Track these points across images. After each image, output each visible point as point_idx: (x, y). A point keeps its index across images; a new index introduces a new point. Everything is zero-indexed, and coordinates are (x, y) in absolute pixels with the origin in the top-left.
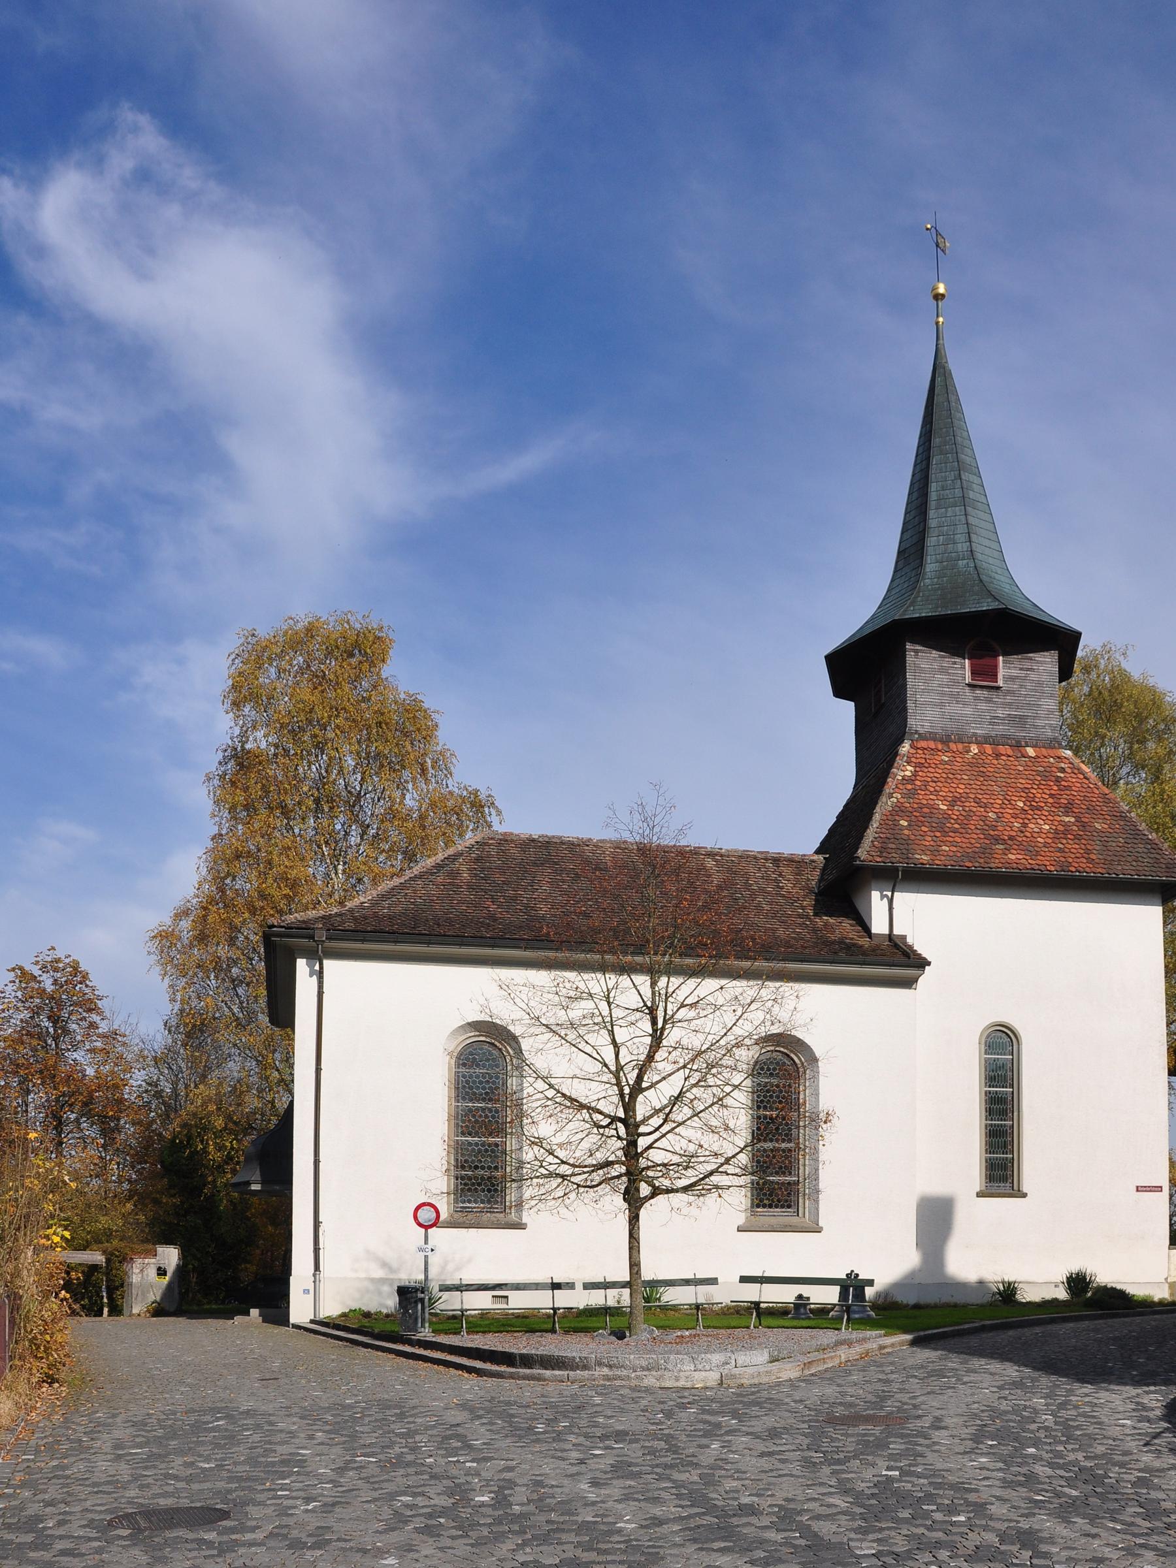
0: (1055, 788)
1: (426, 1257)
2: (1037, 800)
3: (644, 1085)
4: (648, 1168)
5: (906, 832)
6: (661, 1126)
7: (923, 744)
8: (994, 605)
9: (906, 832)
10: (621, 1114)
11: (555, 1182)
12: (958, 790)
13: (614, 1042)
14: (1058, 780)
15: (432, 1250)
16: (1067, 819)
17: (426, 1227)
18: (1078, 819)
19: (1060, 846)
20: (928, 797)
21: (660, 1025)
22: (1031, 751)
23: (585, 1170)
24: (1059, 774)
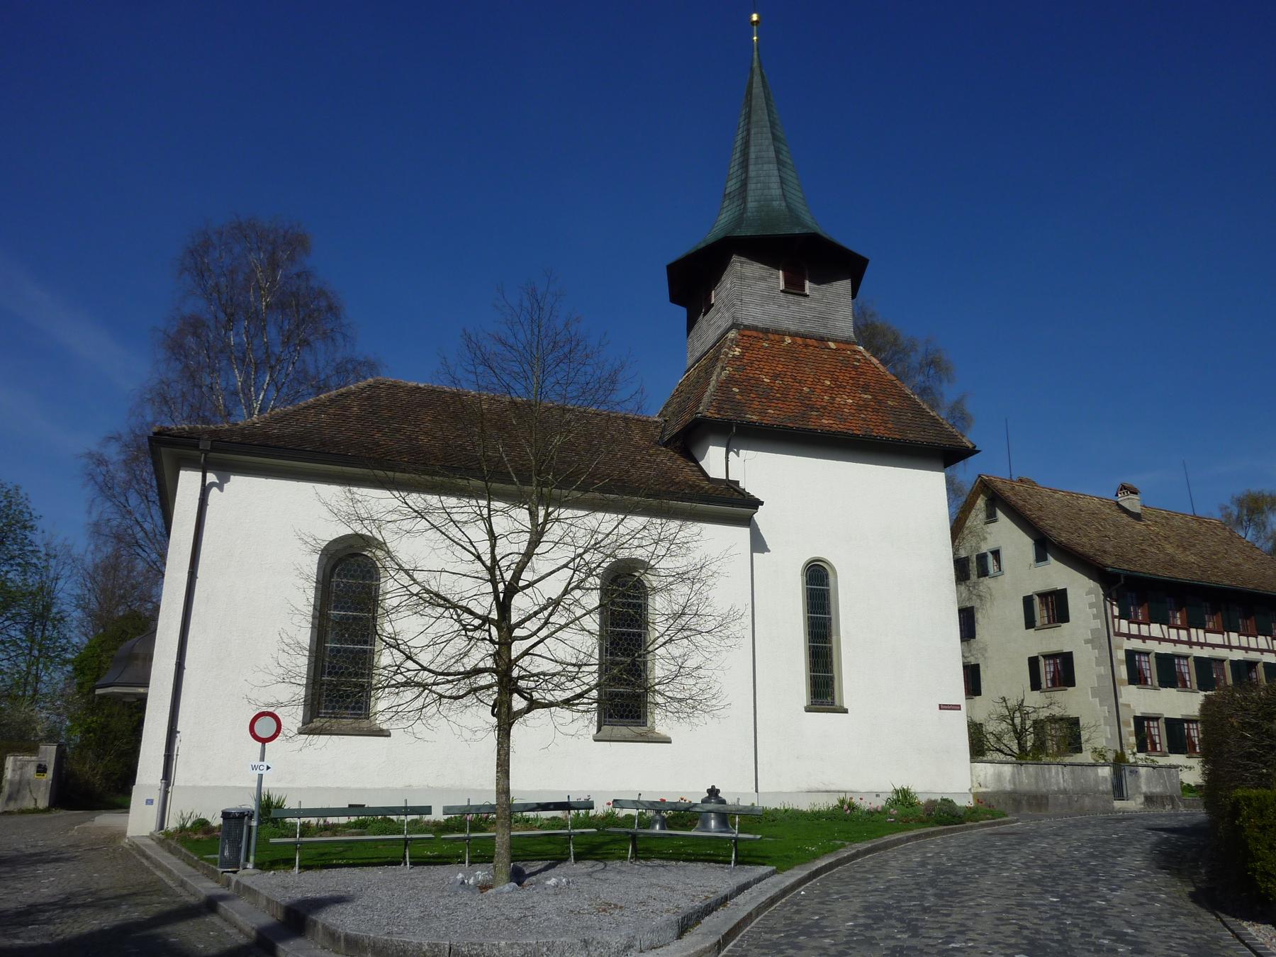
0: (854, 373)
1: (261, 776)
2: (840, 380)
3: (521, 583)
4: (522, 678)
5: (738, 397)
6: (539, 629)
7: (747, 333)
8: (805, 231)
9: (738, 397)
10: (494, 615)
11: (409, 694)
12: (777, 368)
13: (491, 532)
14: (855, 367)
15: (268, 768)
16: (866, 396)
17: (264, 741)
18: (875, 398)
19: (863, 416)
20: (753, 372)
21: (541, 520)
22: (832, 345)
23: (450, 678)
24: (855, 363)
